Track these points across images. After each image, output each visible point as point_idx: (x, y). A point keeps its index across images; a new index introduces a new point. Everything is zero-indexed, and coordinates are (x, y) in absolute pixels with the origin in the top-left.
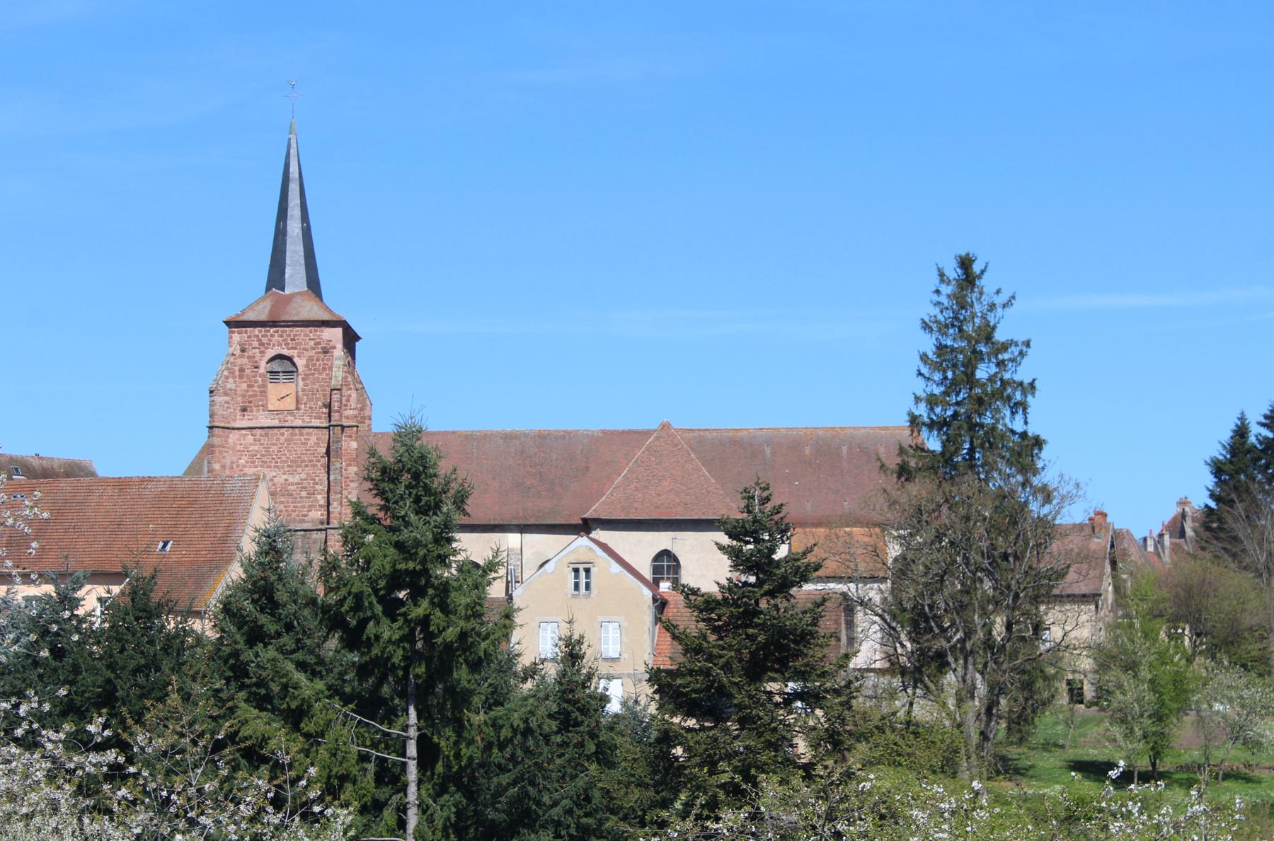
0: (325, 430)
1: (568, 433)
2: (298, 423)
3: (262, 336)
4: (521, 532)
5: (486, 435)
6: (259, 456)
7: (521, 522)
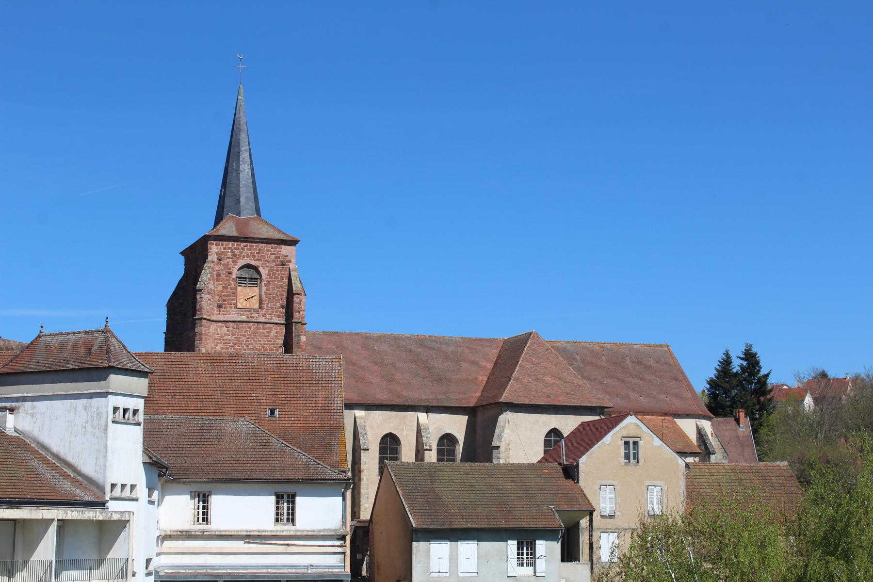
2: (262, 319)
5: (380, 337)
6: (231, 344)
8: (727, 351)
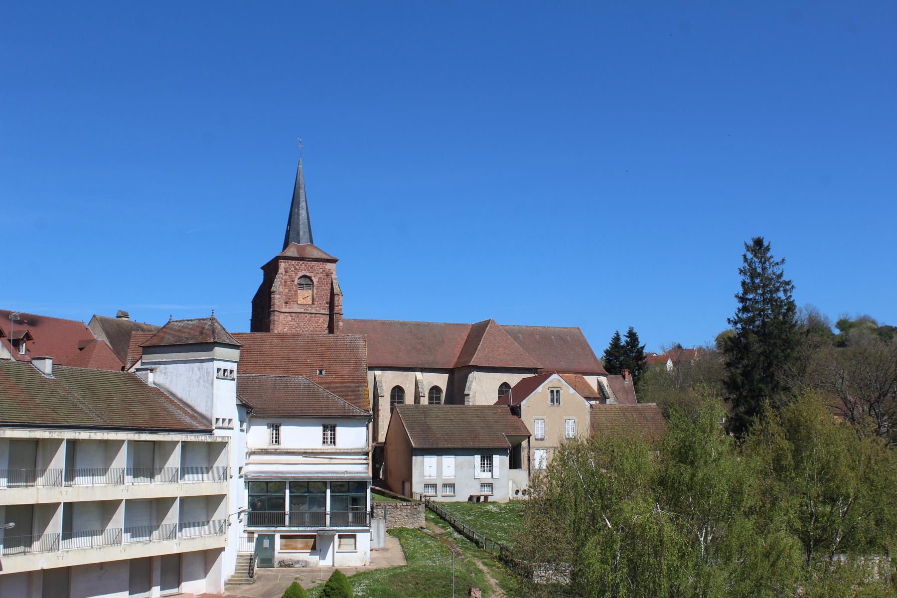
1: (429, 323)
2: (314, 311)
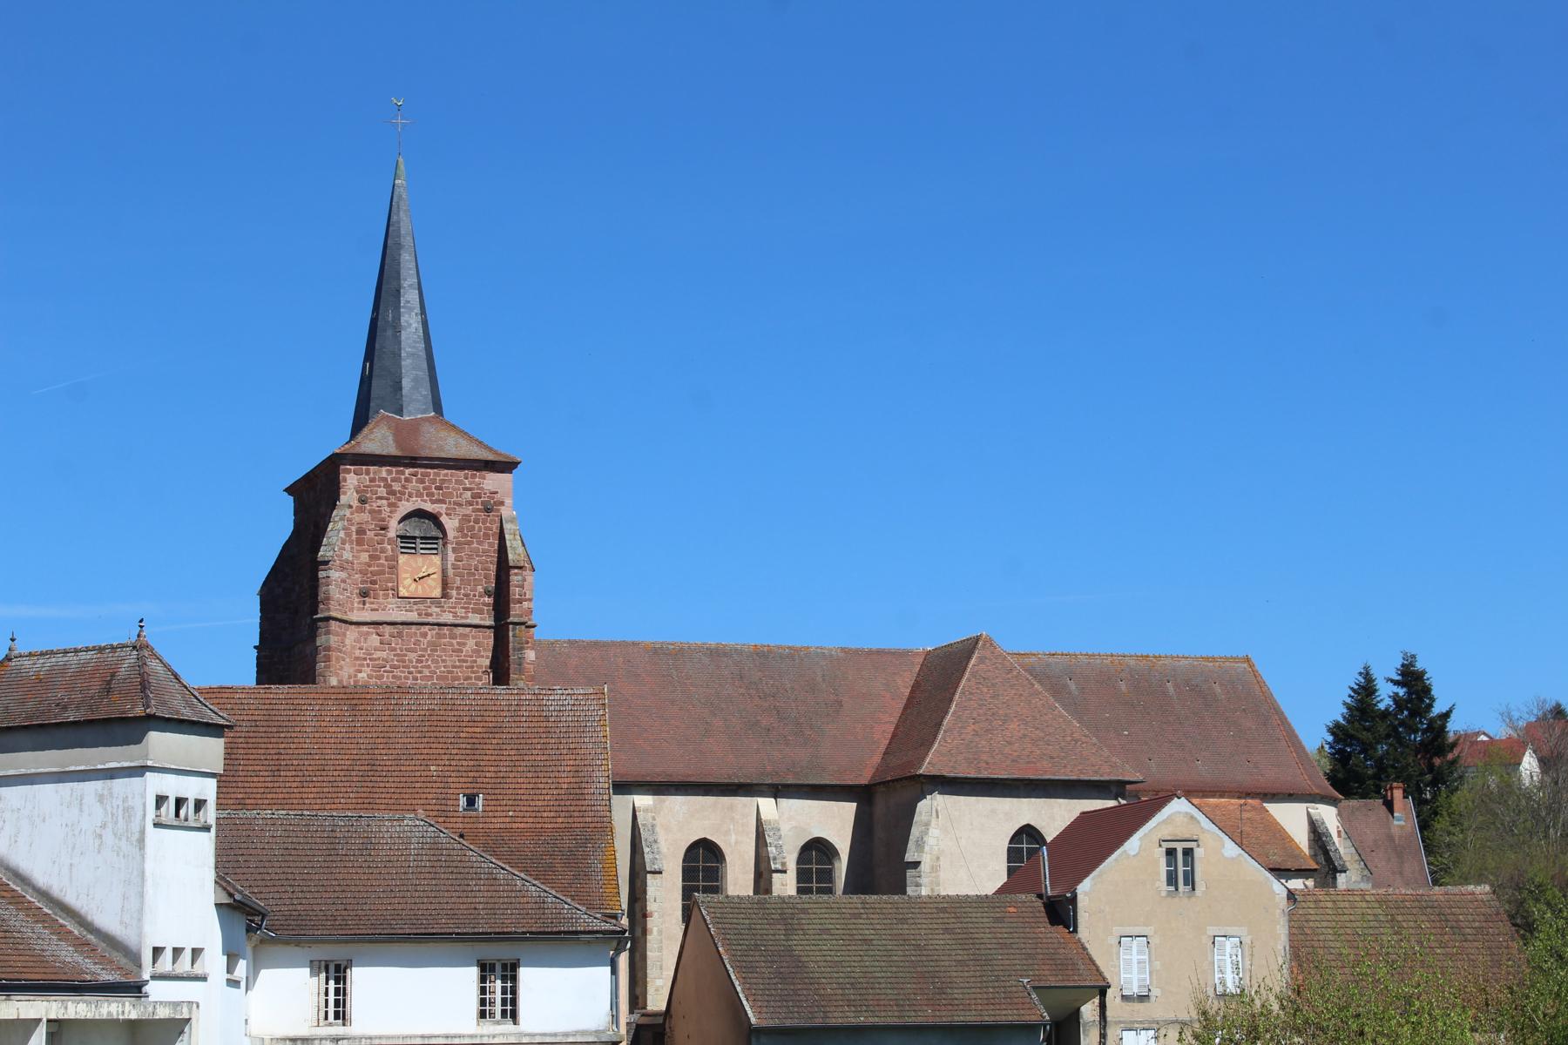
0: (488, 631)
1: (797, 650)
2: (448, 618)
3: (393, 480)
4: (655, 793)
5: (682, 649)
6: (388, 668)
7: (776, 781)
8: (1367, 668)
